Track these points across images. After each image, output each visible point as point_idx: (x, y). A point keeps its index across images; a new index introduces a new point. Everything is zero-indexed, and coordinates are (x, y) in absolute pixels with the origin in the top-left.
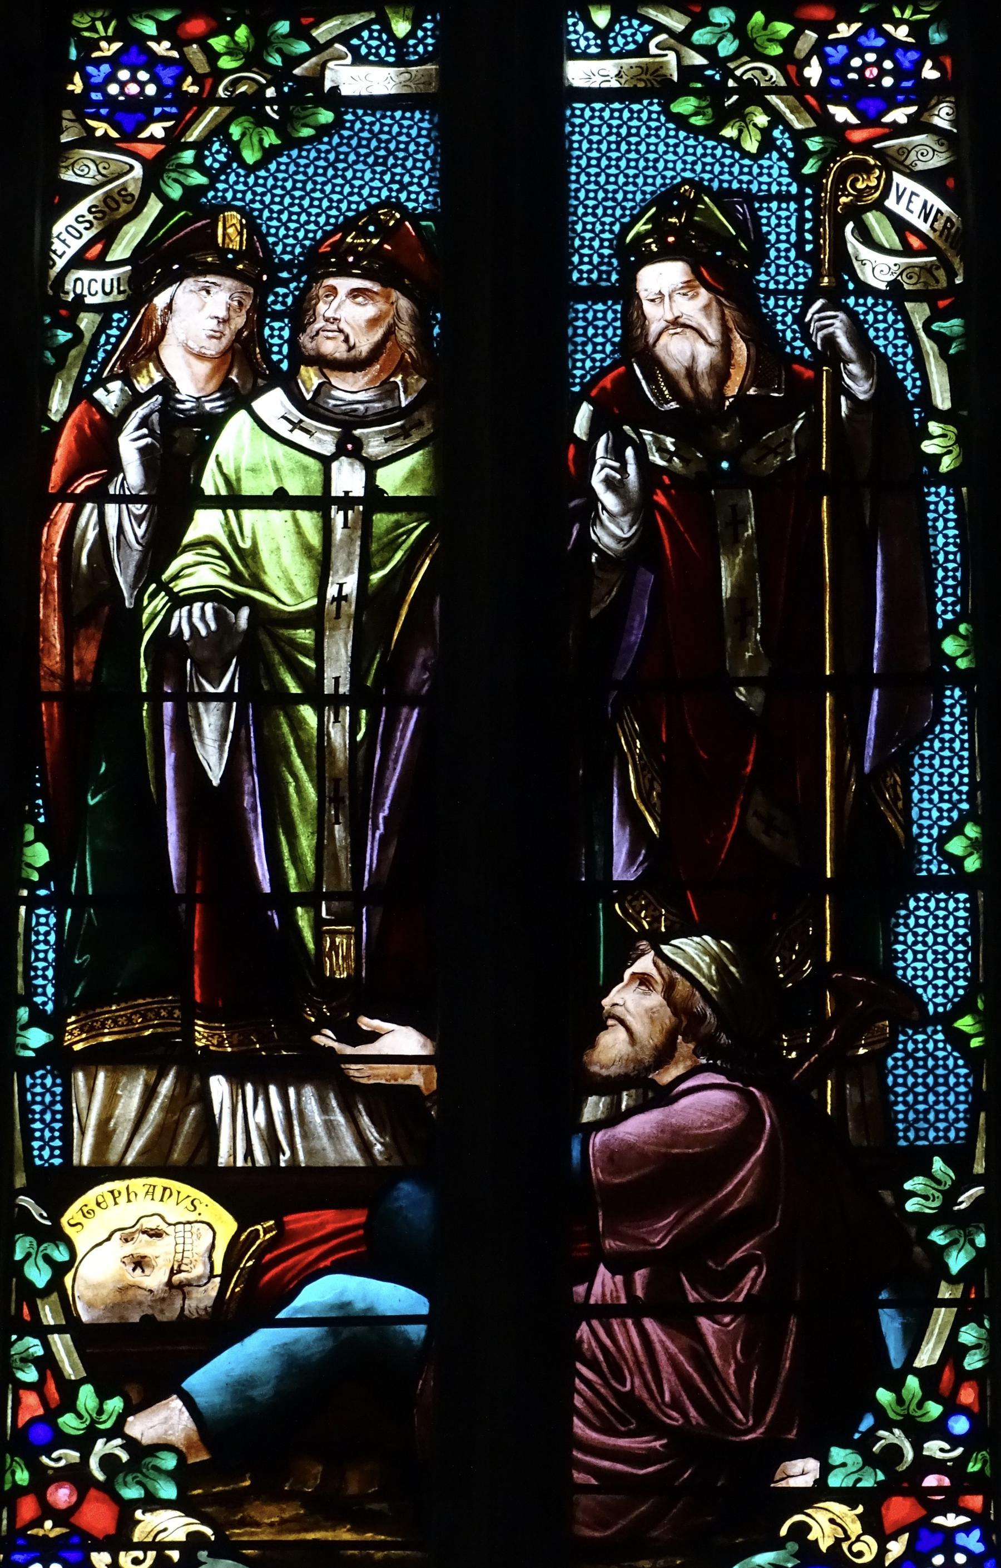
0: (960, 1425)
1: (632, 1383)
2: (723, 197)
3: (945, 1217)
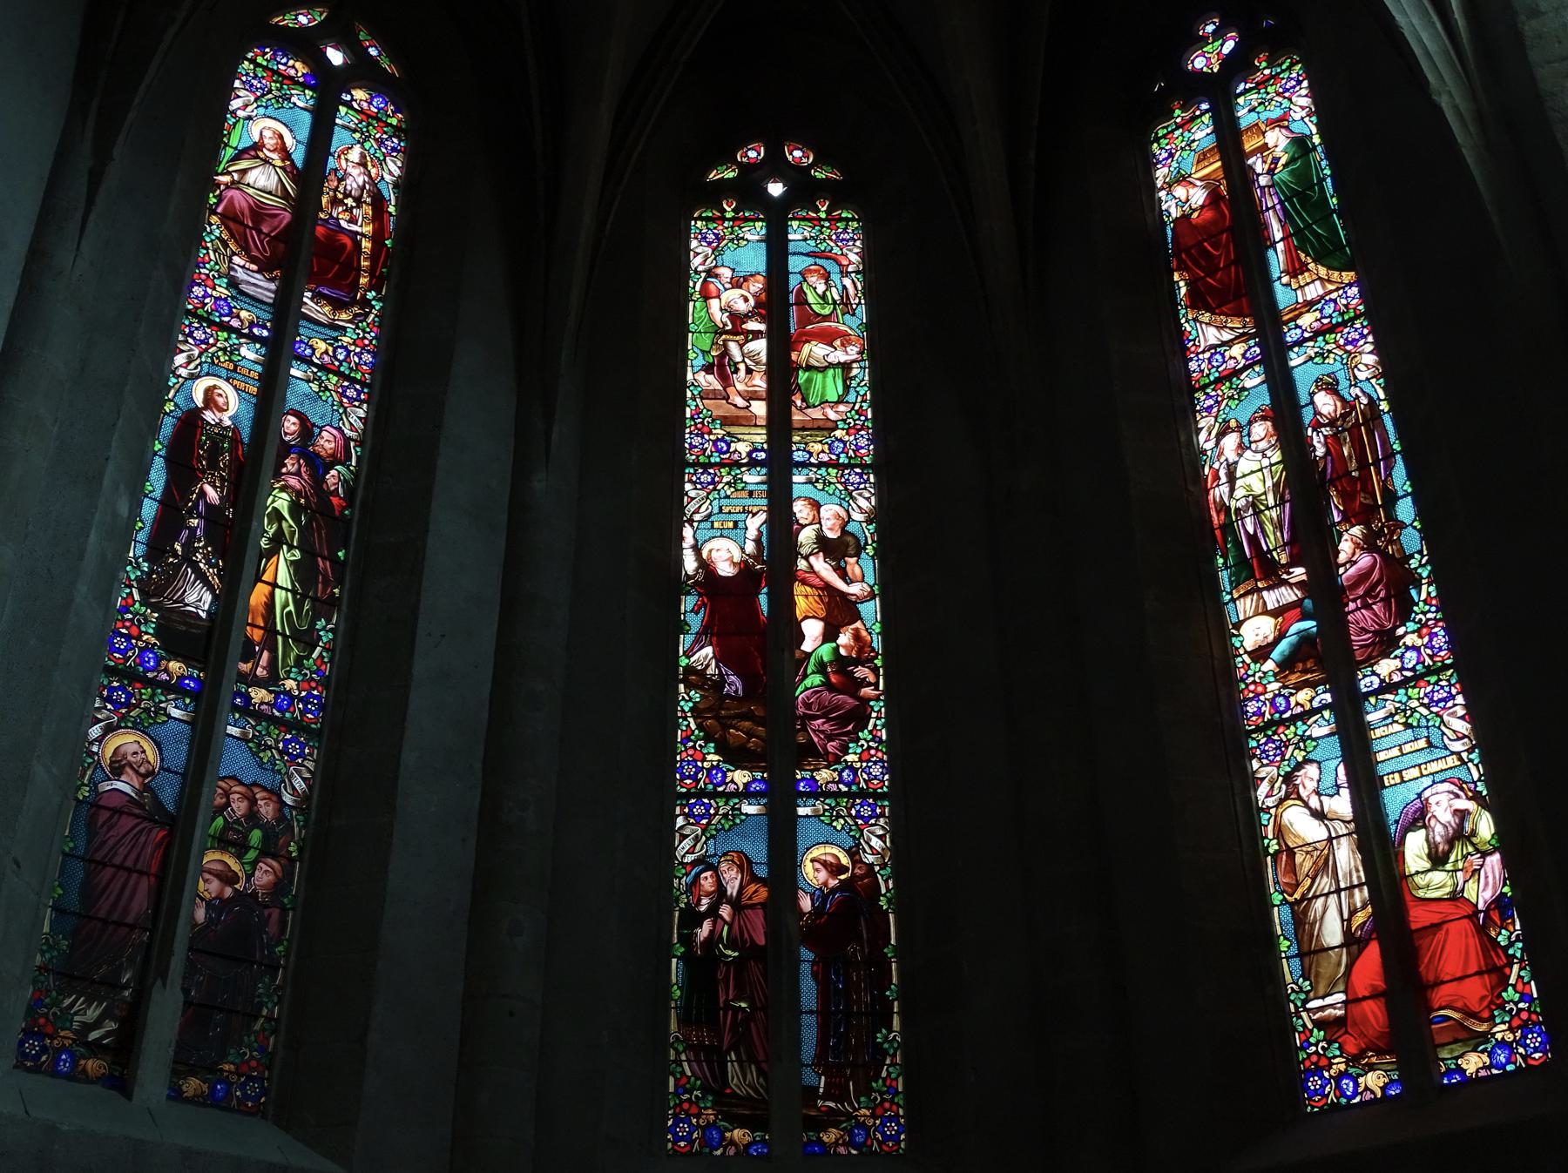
0: (1433, 609)
1: (1362, 625)
2: (1328, 375)
3: (1421, 566)
